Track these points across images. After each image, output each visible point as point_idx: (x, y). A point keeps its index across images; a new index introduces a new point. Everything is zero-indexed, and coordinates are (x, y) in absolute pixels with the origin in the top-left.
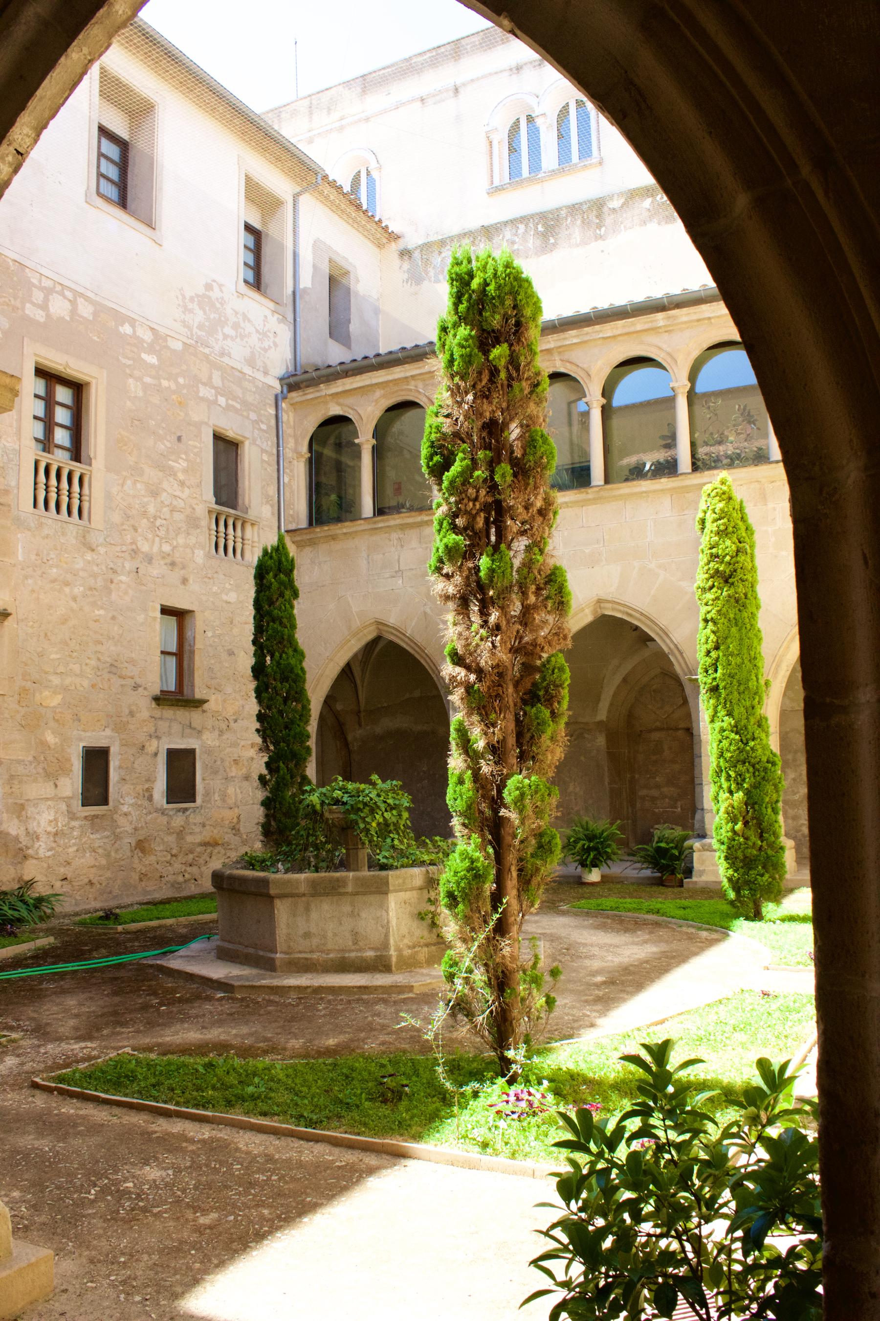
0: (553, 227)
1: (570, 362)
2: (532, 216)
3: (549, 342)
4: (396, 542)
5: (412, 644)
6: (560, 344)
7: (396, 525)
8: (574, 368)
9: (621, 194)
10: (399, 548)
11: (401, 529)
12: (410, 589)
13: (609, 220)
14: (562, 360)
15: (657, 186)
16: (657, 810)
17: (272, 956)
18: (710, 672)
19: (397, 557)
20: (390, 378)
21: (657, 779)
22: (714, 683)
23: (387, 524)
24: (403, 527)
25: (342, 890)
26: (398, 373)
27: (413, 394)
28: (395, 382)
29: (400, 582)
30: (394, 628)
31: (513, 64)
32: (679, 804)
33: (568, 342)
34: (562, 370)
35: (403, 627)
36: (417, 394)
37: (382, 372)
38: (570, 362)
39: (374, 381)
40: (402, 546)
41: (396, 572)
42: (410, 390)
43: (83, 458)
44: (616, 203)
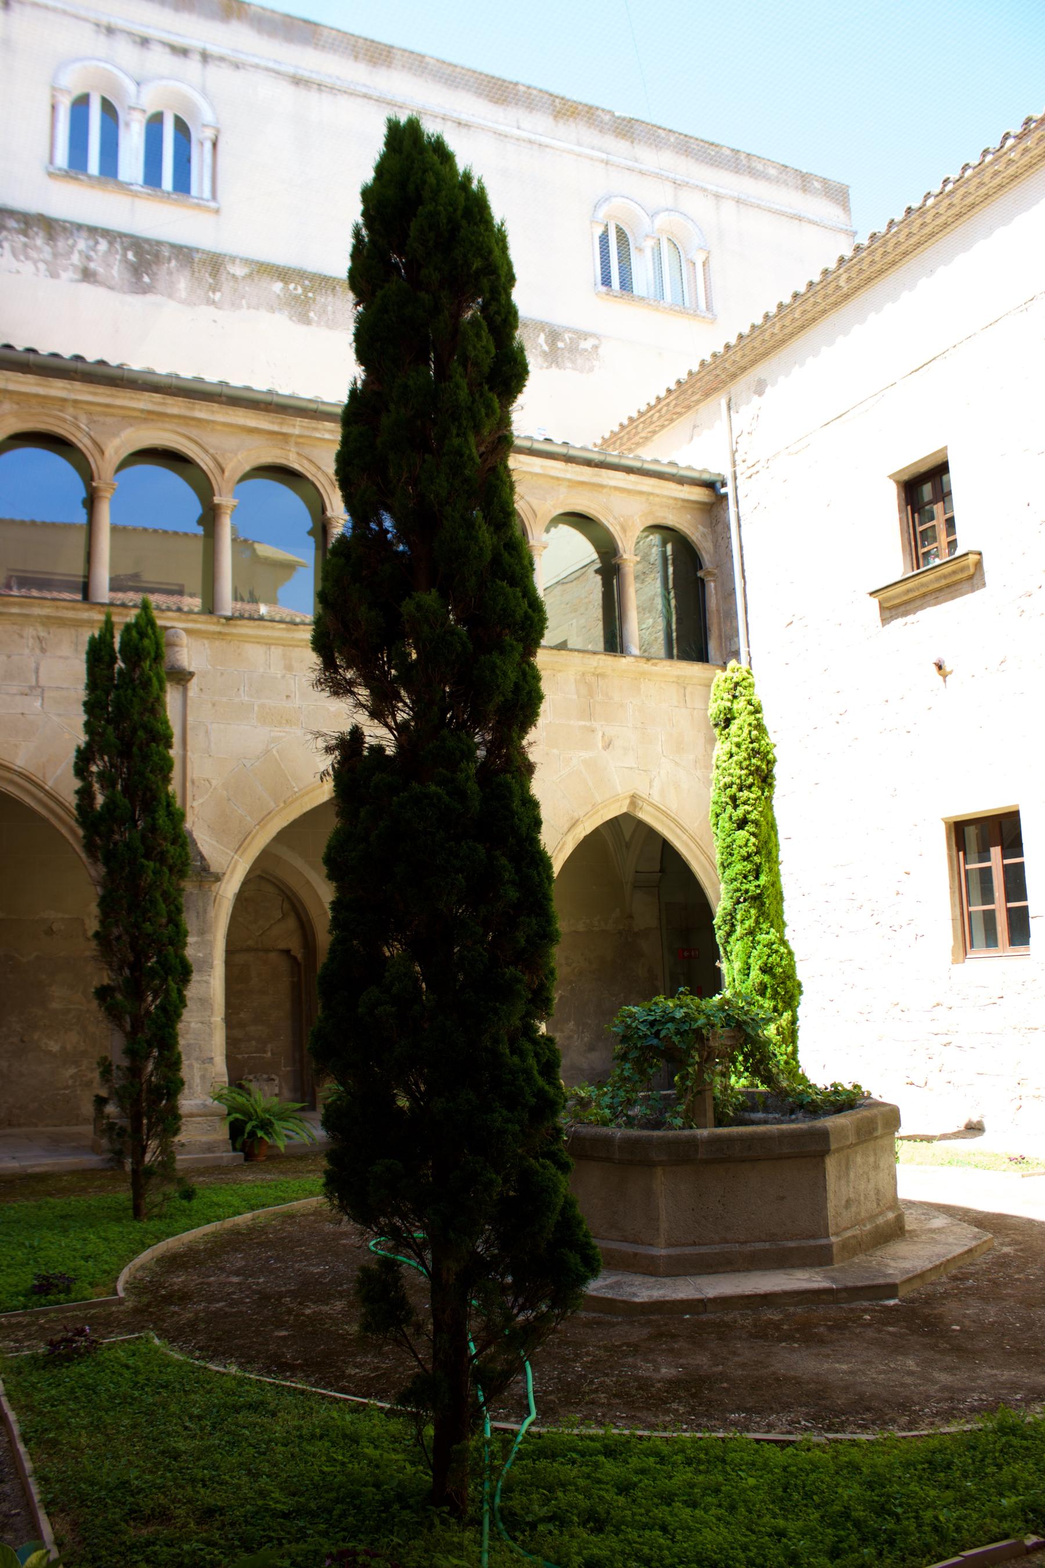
0: (149, 264)
1: (310, 461)
2: (122, 235)
3: (294, 426)
4: (31, 641)
5: (52, 804)
6: (306, 433)
7: (39, 616)
8: (313, 470)
9: (247, 262)
10: (38, 652)
11: (44, 624)
12: (55, 718)
13: (227, 286)
14: (298, 454)
15: (347, 282)
16: (240, 1056)
17: (823, 1242)
18: (751, 878)
19: (33, 665)
20: (41, 391)
21: (242, 1015)
22: (758, 891)
23: (25, 611)
24: (48, 621)
25: (875, 1134)
26: (58, 388)
27: (67, 427)
28: (44, 400)
29: (38, 704)
30: (20, 774)
31: (104, 20)
32: (269, 1047)
33: (318, 435)
34: (296, 466)
35: (40, 776)
36: (73, 430)
37: (31, 378)
38: (310, 461)
39: (11, 387)
40: (43, 650)
41: (31, 688)
42: (64, 420)
43: (939, 461)
44: (239, 271)
